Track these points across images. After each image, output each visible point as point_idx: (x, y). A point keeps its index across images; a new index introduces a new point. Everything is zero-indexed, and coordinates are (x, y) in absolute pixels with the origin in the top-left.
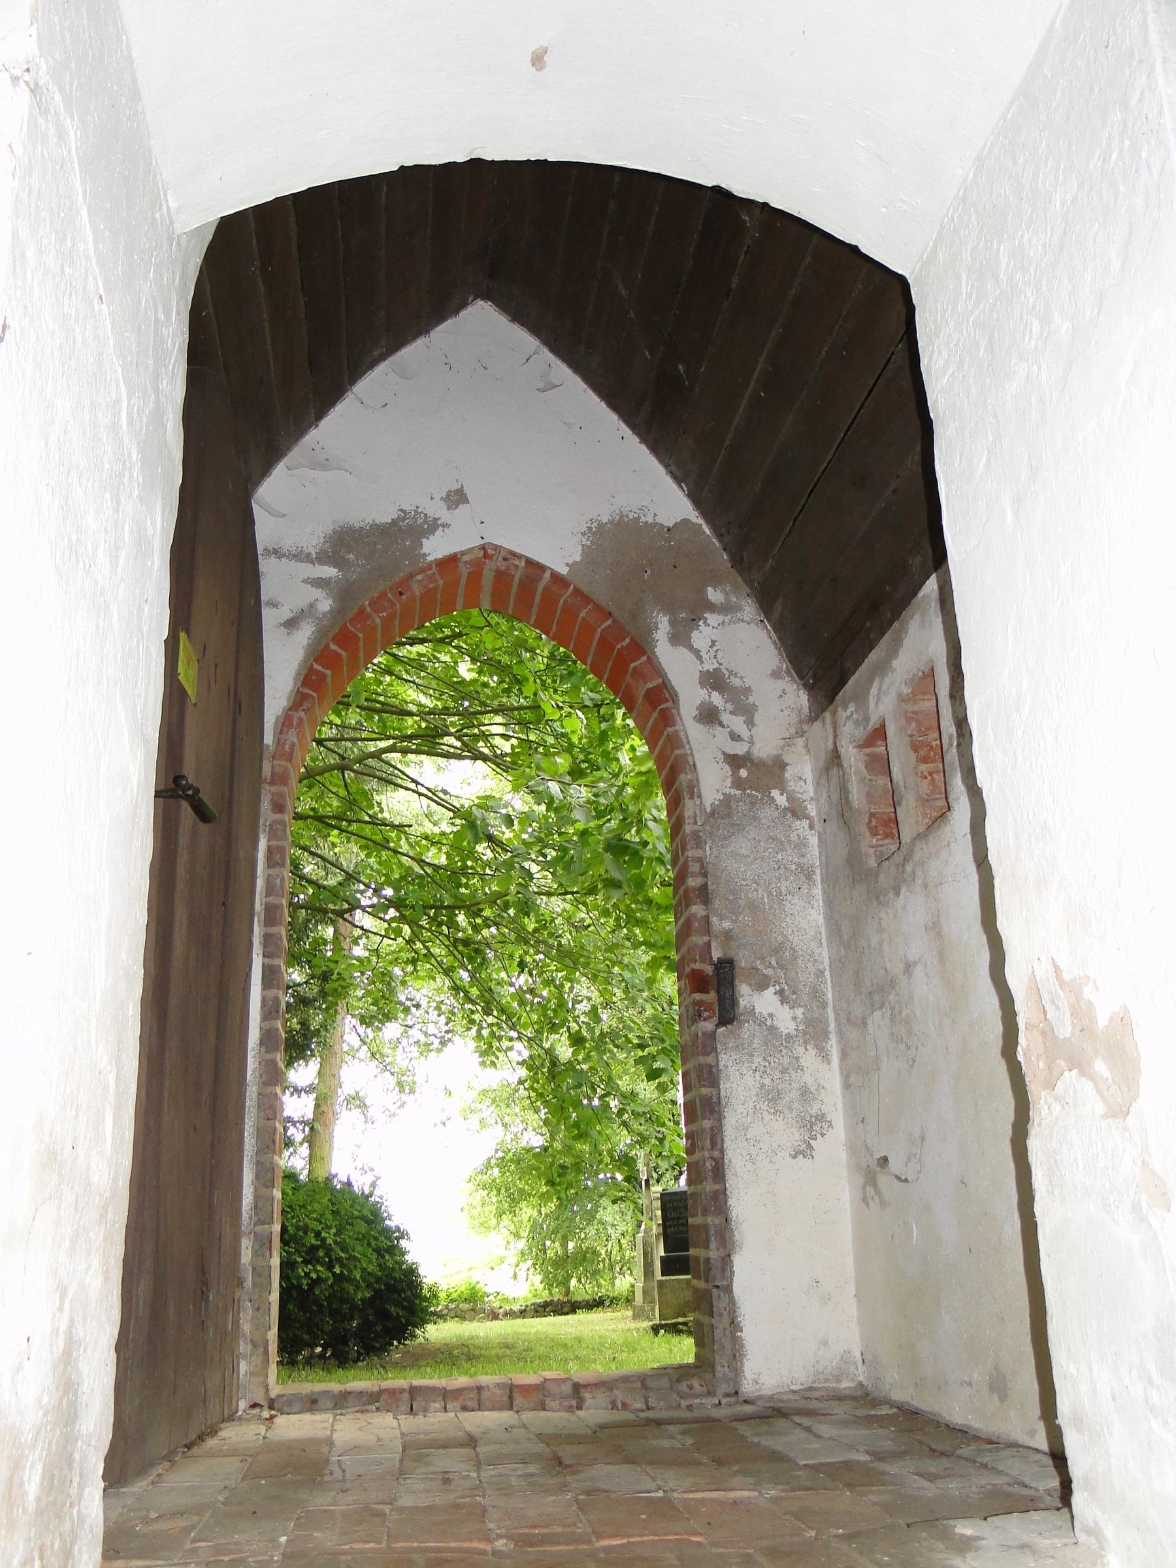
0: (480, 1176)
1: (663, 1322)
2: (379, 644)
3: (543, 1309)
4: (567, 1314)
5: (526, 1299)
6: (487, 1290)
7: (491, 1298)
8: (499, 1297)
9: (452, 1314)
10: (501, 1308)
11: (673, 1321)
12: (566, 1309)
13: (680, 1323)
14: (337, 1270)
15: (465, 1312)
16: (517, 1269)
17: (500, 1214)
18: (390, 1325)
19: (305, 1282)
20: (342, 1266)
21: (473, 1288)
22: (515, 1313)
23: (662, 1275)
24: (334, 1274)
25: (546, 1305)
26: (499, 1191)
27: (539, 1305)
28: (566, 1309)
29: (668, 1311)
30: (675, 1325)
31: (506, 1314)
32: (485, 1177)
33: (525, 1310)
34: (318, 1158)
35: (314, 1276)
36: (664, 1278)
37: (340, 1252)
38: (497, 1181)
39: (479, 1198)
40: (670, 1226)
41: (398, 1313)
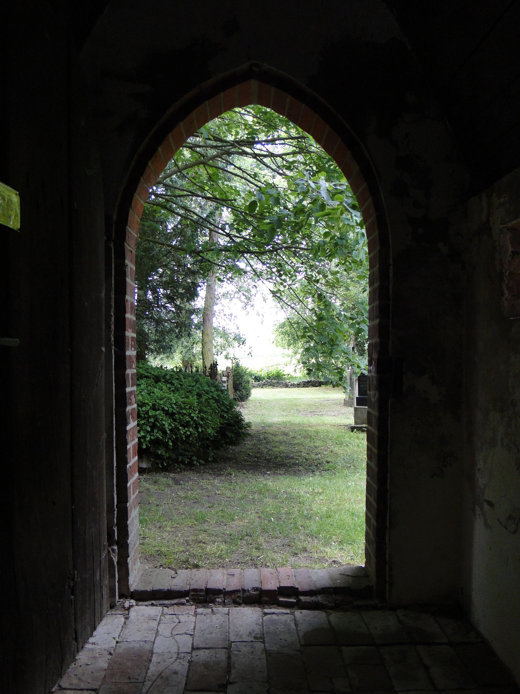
0: (281, 329)
1: (356, 426)
2: (184, 134)
3: (306, 384)
4: (317, 386)
5: (300, 378)
6: (284, 373)
7: (286, 376)
8: (289, 376)
9: (269, 384)
10: (289, 382)
11: (360, 426)
12: (317, 384)
13: (364, 427)
14: (200, 430)
15: (274, 383)
16: (296, 368)
17: (289, 345)
18: (228, 440)
19: (184, 436)
20: (202, 427)
21: (278, 373)
22: (295, 385)
23: (357, 405)
24: (198, 432)
25: (308, 382)
26: (289, 335)
27: (305, 382)
28: (317, 384)
29: (359, 421)
30: (361, 428)
31: (291, 385)
32: (283, 330)
33: (299, 384)
34: (206, 334)
35: (189, 433)
36: (357, 407)
37: (201, 422)
38: (288, 331)
39: (280, 337)
40: (362, 384)
41: (231, 436)
